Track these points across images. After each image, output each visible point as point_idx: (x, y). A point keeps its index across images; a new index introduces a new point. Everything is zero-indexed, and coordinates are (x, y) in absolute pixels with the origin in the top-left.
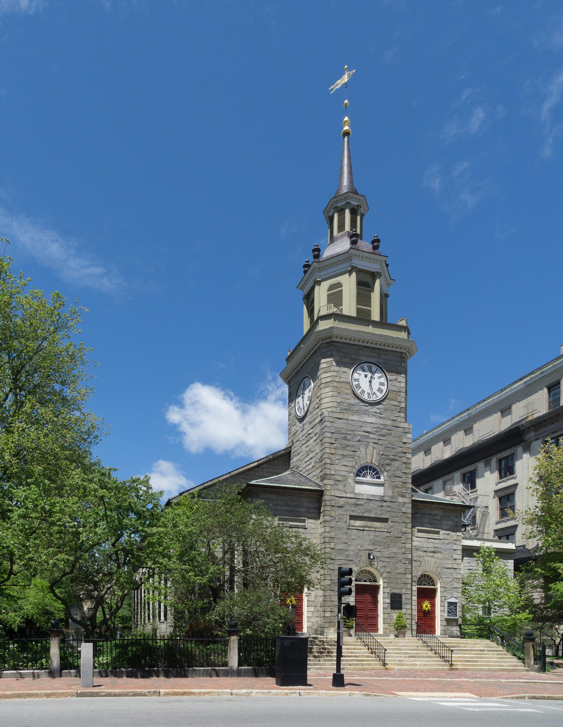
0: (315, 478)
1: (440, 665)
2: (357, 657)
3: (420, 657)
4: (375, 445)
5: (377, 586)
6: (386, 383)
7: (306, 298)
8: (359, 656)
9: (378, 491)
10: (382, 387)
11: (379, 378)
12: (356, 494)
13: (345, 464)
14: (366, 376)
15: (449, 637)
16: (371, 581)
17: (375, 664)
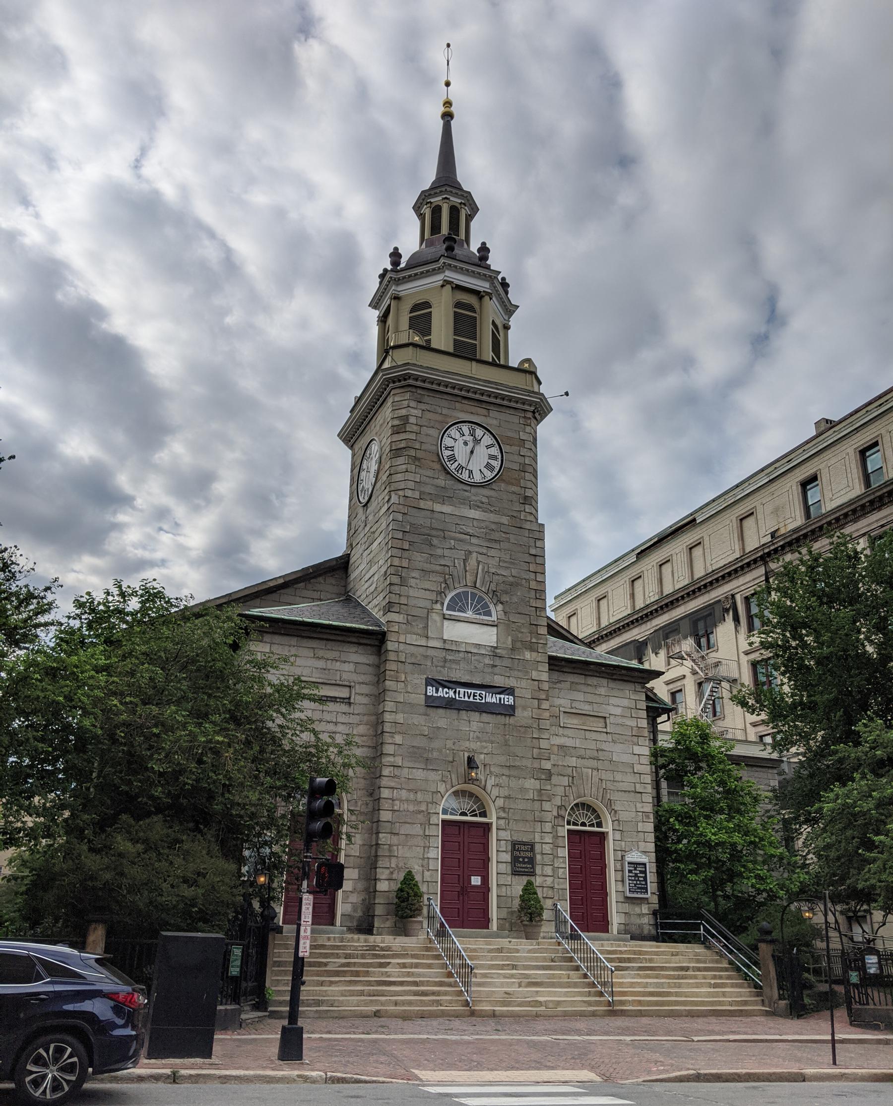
0: (376, 609)
1: (589, 1003)
2: (416, 984)
3: (553, 985)
4: (480, 558)
5: (603, 833)
6: (500, 457)
7: (382, 321)
8: (422, 983)
9: (487, 637)
10: (492, 462)
11: (488, 447)
12: (445, 641)
13: (426, 587)
14: (466, 443)
15: (632, 938)
16: (475, 815)
17: (450, 1002)
